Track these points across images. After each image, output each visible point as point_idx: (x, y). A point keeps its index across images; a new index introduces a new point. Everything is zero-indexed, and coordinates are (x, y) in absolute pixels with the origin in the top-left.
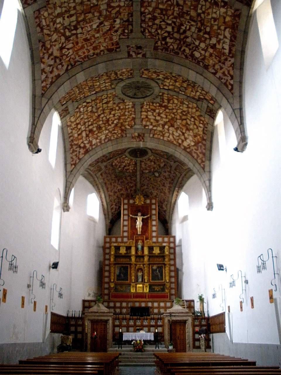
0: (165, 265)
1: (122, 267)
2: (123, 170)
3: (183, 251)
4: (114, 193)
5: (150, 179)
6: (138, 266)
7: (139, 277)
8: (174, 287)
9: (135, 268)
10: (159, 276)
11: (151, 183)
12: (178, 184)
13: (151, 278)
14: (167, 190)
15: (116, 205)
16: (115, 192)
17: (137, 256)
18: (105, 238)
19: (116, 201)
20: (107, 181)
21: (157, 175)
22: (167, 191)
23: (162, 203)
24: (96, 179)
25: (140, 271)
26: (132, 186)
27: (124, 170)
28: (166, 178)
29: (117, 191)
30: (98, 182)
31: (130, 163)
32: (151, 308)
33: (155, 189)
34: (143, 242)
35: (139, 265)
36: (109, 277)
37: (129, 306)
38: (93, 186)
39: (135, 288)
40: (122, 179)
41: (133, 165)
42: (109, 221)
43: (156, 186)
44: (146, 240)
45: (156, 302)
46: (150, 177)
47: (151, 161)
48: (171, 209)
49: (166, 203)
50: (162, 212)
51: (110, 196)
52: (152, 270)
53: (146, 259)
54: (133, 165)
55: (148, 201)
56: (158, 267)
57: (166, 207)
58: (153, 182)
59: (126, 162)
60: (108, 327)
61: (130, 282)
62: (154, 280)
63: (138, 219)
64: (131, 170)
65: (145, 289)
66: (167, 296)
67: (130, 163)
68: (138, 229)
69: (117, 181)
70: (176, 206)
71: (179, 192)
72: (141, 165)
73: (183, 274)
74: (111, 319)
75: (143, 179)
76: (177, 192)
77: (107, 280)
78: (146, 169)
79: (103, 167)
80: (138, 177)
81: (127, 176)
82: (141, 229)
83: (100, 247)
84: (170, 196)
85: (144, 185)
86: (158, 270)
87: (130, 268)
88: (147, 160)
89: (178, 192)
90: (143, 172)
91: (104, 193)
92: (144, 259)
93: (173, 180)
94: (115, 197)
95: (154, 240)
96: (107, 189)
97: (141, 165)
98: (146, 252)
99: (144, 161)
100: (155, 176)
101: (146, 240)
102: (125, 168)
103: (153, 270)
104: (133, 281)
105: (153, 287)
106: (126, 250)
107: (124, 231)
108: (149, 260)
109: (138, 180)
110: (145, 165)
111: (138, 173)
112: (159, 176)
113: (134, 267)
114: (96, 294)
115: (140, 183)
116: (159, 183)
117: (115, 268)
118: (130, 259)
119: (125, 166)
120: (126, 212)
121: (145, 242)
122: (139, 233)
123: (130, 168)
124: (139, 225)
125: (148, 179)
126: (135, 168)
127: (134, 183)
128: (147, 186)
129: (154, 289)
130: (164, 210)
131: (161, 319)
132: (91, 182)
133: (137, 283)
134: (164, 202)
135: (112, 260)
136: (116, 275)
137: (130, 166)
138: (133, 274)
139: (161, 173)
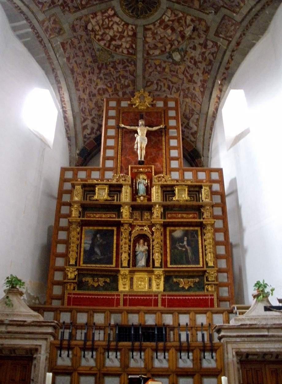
0: (202, 225)
1: (98, 232)
2: (109, 47)
3: (240, 202)
4: (89, 96)
5: (164, 69)
6: (138, 228)
7: (139, 257)
8: (226, 280)
9: (130, 234)
10: (190, 254)
11: (166, 79)
12: (222, 70)
13: (169, 259)
14: (197, 89)
15: (93, 121)
16: (91, 95)
17: (134, 208)
18: (64, 170)
19: (94, 113)
20: (75, 65)
21: (177, 57)
22: (197, 93)
23: (189, 119)
24: (52, 53)
25: (142, 241)
26: (126, 84)
27: (112, 47)
28: (195, 64)
29: (95, 92)
30: (55, 62)
31: (123, 32)
32: (172, 328)
33: (174, 90)
34: (150, 178)
35: (140, 226)
36: (65, 256)
37: (112, 323)
38: (47, 73)
39: (128, 282)
40: (107, 69)
41: (129, 36)
42: (78, 152)
43: (175, 83)
44: (155, 175)
45: (185, 313)
46: (164, 65)
47: (166, 27)
48: (208, 128)
49: (196, 116)
50: (188, 137)
51: (80, 99)
52: (173, 239)
53: (157, 212)
54: (129, 36)
55: (160, 104)
56: (186, 233)
57: (196, 125)
58: (169, 77)
59: (115, 27)
60: (32, 378)
61: (117, 266)
62: (176, 264)
63: (139, 131)
64: (126, 48)
65: (154, 284)
66: (212, 300)
67: (123, 32)
68: (139, 152)
69: (97, 71)
70: (217, 122)
71: (224, 89)
72: (145, 37)
73: (244, 251)
74: (44, 346)
75: (150, 70)
76: (218, 91)
77: (60, 262)
78: (156, 47)
79: (66, 27)
80: (140, 64)
81: (118, 61)
82: (144, 152)
83: (52, 196)
84: (206, 99)
85: (152, 83)
86: (186, 238)
87: (119, 234)
88: (157, 24)
89: (221, 90)
90: (148, 54)
91: (69, 90)
92: (152, 214)
93: (210, 63)
94: (93, 106)
95: (175, 175)
96: (76, 84)
97: (145, 37)
98: (156, 195)
99: (151, 26)
100: (175, 63)
101: (155, 175)
102: (114, 43)
103: (174, 240)
104: (125, 264)
105: (175, 280)
106: (109, 195)
107: (106, 158)
108: (164, 215)
109: (139, 71)
110: (154, 38)
111: (140, 55)
112: (183, 60)
113: (128, 232)
114: (34, 298)
115: (144, 77)
116: (181, 76)
117: (80, 233)
118: (120, 215)
119: (113, 39)
120: (112, 122)
121: (155, 177)
122: (141, 154)
123: (124, 45)
124: (141, 143)
125: (158, 69)
126: (134, 46)
127: (132, 77)
128: (157, 84)
129: (178, 284)
130: (193, 131)
131: (213, 349)
132: (41, 63)
133: (134, 269)
134: (193, 115)
135: (75, 213)
136: (82, 250)
137: (124, 40)
138: (125, 248)
139: (186, 52)
